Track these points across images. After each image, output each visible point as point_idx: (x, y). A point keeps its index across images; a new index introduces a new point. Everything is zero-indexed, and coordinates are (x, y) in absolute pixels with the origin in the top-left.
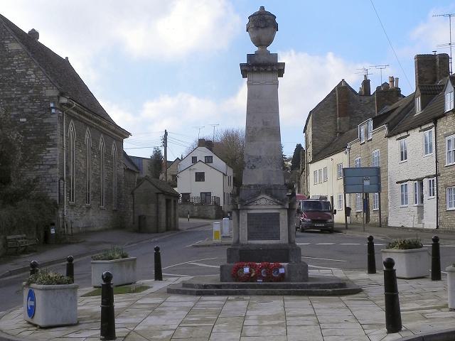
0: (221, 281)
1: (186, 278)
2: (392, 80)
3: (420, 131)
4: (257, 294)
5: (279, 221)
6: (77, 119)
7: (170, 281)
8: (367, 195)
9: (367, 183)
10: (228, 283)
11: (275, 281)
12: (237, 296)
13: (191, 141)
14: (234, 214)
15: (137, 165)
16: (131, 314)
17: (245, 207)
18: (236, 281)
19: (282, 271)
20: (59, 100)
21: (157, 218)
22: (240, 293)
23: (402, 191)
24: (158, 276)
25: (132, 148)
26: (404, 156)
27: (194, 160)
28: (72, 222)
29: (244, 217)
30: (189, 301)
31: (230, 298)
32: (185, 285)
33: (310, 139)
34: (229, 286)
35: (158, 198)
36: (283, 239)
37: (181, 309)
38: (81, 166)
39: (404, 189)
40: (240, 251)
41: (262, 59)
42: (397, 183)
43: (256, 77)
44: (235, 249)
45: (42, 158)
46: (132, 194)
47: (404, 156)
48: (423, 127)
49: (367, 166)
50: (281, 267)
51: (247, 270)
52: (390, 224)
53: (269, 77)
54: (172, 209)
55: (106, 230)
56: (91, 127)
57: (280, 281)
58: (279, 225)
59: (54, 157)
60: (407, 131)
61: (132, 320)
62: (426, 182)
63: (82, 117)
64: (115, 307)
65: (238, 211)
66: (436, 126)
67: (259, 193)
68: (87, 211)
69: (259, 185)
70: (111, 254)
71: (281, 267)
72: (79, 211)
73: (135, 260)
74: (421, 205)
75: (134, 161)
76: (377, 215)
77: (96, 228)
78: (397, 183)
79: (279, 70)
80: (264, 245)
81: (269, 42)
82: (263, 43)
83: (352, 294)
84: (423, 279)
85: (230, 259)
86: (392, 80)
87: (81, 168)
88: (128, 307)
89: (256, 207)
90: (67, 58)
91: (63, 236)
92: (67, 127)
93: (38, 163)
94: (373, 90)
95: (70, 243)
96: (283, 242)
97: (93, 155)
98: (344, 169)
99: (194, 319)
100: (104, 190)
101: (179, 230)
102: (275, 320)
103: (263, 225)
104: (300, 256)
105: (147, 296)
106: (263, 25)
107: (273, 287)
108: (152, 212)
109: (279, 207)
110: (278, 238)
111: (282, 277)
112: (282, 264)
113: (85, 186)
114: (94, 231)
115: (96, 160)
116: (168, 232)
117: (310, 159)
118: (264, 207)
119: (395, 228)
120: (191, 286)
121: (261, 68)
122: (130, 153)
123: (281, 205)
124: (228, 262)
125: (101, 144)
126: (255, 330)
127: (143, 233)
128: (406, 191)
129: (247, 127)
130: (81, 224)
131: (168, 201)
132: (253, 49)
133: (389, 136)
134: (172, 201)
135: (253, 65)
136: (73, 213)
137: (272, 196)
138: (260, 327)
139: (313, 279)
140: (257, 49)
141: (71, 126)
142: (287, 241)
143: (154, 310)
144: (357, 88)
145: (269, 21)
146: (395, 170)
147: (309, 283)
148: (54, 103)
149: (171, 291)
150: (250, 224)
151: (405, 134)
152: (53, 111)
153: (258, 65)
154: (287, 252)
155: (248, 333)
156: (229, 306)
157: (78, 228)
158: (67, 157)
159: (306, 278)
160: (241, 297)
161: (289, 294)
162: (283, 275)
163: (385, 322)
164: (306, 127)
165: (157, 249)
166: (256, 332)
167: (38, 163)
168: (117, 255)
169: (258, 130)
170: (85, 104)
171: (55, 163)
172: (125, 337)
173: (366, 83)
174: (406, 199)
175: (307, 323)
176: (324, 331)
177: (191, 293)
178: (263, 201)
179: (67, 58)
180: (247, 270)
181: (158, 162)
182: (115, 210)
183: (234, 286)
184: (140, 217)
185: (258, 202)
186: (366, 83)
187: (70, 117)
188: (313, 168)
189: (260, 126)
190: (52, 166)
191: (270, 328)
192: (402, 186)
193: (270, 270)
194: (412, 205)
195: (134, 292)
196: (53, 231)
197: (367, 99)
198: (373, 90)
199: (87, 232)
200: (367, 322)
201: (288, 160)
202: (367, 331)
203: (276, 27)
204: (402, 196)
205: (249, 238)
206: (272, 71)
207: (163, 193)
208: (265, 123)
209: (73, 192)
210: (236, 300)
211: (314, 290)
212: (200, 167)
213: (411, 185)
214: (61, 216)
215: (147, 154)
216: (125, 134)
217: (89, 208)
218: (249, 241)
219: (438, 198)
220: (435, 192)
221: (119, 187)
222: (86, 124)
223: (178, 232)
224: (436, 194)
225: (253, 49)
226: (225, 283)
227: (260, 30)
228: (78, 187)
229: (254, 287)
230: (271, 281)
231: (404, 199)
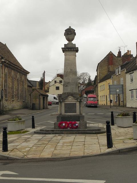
0: (55, 129)
1: (43, 127)
2: (128, 51)
4: (67, 133)
5: (76, 106)
6: (8, 67)
7: (38, 129)
8: (119, 95)
9: (118, 91)
10: (56, 129)
11: (74, 129)
12: (54, 135)
13: (55, 75)
14: (60, 103)
15: (33, 84)
16: (17, 142)
17: (64, 101)
18: (60, 129)
19: (77, 125)
21: (40, 104)
22: (60, 133)
23: (131, 94)
24: (33, 127)
25: (31, 77)
26: (132, 80)
27: (55, 82)
28: (6, 106)
29: (63, 104)
30: (40, 136)
31: (57, 135)
32: (41, 130)
34: (57, 131)
35: (40, 97)
36: (78, 113)
37: (36, 139)
38: (10, 85)
39: (132, 93)
40: (62, 117)
41: (70, 46)
42: (130, 90)
43: (68, 53)
44: (60, 117)
46: (30, 95)
47: (132, 80)
50: (77, 123)
51: (64, 124)
52: (127, 106)
53: (72, 53)
54: (46, 101)
55: (20, 109)
56: (14, 70)
57: (76, 129)
58: (76, 107)
60: (133, 71)
61: (16, 144)
63: (10, 66)
64: (8, 141)
65: (61, 102)
67: (68, 96)
68: (12, 102)
69: (69, 93)
70: (15, 119)
71: (77, 123)
72: (9, 102)
73: (24, 121)
75: (32, 83)
76: (122, 102)
77: (16, 108)
78: (130, 90)
79: (77, 50)
81: (73, 39)
82: (70, 40)
83: (103, 133)
84: (131, 128)
85: (58, 121)
88: (17, 139)
89: (68, 101)
91: (2, 112)
92: (5, 70)
95: (5, 114)
96: (78, 114)
99: (39, 143)
101: (48, 109)
102: (69, 143)
103: (70, 108)
104: (84, 118)
105: (26, 135)
107: (73, 131)
108: (38, 102)
109: (76, 101)
111: (77, 127)
112: (77, 122)
114: (15, 110)
116: (44, 110)
117: (99, 82)
118: (71, 101)
119: (129, 108)
120: (43, 131)
121: (70, 49)
122: (29, 79)
124: (57, 121)
125: (18, 76)
126: (60, 147)
127: (34, 110)
128: (133, 94)
129: (64, 71)
130: (10, 107)
131: (44, 98)
132: (66, 42)
133: (126, 73)
134: (46, 98)
135: (66, 48)
137: (73, 97)
138: (63, 146)
139: (89, 127)
140: (68, 42)
141: (6, 70)
142: (79, 114)
143: (26, 140)
144: (116, 54)
145: (72, 32)
147: (86, 129)
149: (35, 133)
151: (132, 72)
153: (68, 48)
154: (79, 118)
155: (57, 149)
156: (55, 138)
157: (9, 108)
159: (86, 127)
160: (61, 135)
161: (79, 133)
162: (77, 126)
163: (107, 144)
164: (97, 70)
165: (33, 117)
166: (60, 148)
168: (17, 119)
169: (68, 72)
170: (12, 62)
172: (12, 151)
173: (120, 53)
174: (133, 96)
175: (80, 144)
176: (101, 148)
177: (43, 133)
178: (70, 99)
180: (64, 124)
181: (42, 83)
183: (59, 131)
184: (33, 104)
186: (120, 53)
187: (6, 66)
188: (99, 85)
189: (69, 71)
191: (66, 147)
193: (73, 124)
195: (22, 133)
197: (120, 59)
198: (122, 54)
199: (13, 110)
200: (103, 144)
201: (92, 82)
202: (101, 148)
203: (75, 34)
204: (131, 95)
205: (65, 113)
206: (74, 51)
207: (42, 95)
208: (71, 70)
209: (7, 95)
210: (59, 136)
211: (88, 132)
212: (57, 85)
214: (2, 104)
215: (38, 79)
216: (28, 73)
217: (13, 101)
218: (65, 114)
221: (26, 92)
222: (12, 69)
223: (47, 110)
225: (66, 42)
226: (55, 130)
227: (69, 35)
228: (9, 93)
229: (66, 131)
230: (73, 129)
231: (132, 96)
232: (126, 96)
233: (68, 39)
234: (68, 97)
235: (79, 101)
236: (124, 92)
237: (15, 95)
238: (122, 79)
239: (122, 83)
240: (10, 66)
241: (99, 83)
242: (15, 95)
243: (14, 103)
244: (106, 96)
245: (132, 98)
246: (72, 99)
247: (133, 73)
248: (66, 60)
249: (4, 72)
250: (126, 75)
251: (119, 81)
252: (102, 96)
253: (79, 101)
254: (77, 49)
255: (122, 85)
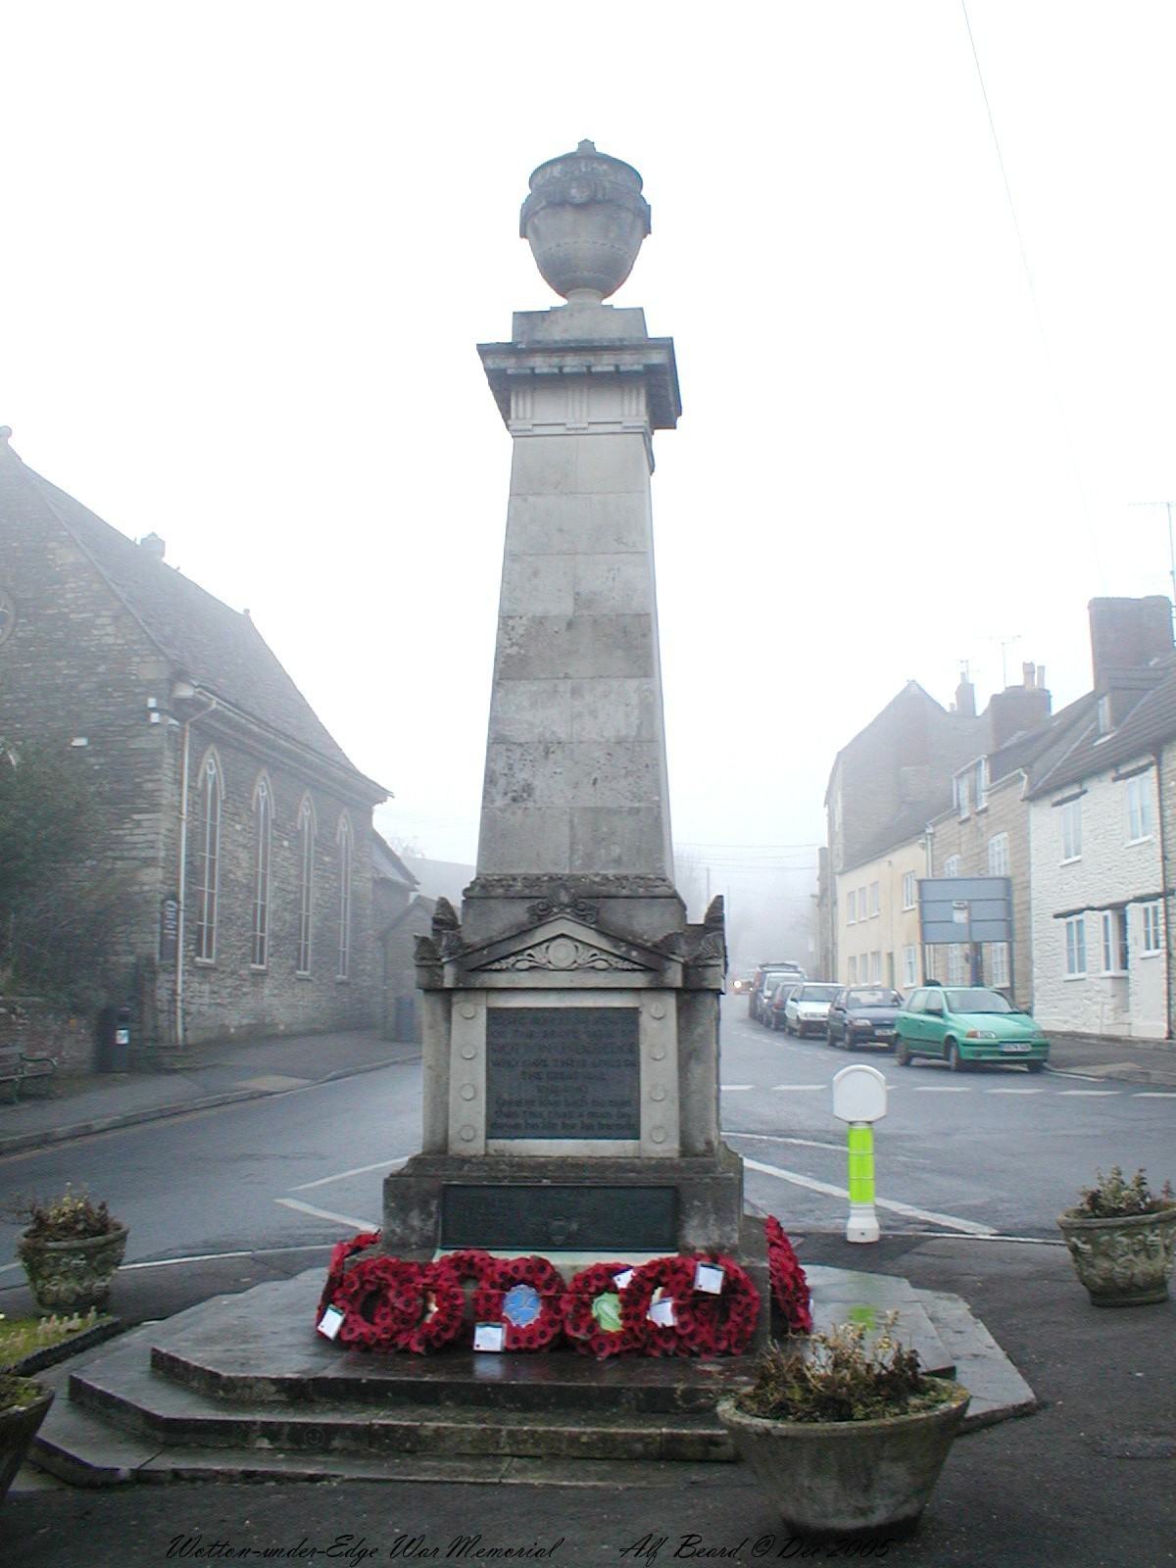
3: (1115, 780)
5: (633, 1049)
8: (977, 947)
20: (171, 691)
33: (839, 819)
36: (657, 1137)
38: (238, 865)
42: (1057, 916)
45: (119, 840)
48: (1123, 770)
49: (976, 876)
58: (635, 1065)
59: (151, 837)
60: (1079, 780)
62: (1134, 913)
66: (1159, 763)
72: (229, 982)
74: (1123, 973)
80: (563, 1163)
86: (1029, 670)
87: (240, 873)
90: (247, 611)
93: (110, 853)
94: (982, 704)
97: (280, 839)
98: (920, 882)
100: (311, 931)
106: (588, 209)
109: (639, 980)
110: (630, 1129)
113: (249, 918)
115: (288, 854)
123: (646, 969)
128: (1080, 941)
130: (235, 1019)
133: (1033, 798)
136: (206, 987)
144: (947, 699)
146: (1050, 887)
148: (159, 697)
150: (498, 1057)
151: (1075, 790)
152: (155, 717)
158: (191, 839)
167: (110, 853)
171: (150, 853)
173: (966, 692)
178: (561, 954)
179: (247, 611)
182: (342, 983)
185: (539, 955)
186: (966, 692)
190: (149, 862)
192: (1070, 923)
194: (1099, 970)
196: (122, 1037)
205: (494, 1130)
213: (1093, 922)
216: (380, 794)
219: (1169, 955)
220: (1162, 937)
224: (1163, 944)
228: (227, 921)
232: (1028, 958)
233: (558, 273)
234: (540, 935)
235: (679, 983)
236: (1017, 925)
237: (275, 936)
238: (999, 845)
239: (999, 862)
240: (247, 741)
241: (841, 874)
242: (275, 936)
243: (267, 992)
244: (890, 956)
245: (1071, 970)
246: (585, 956)
247: (1076, 797)
248: (525, 485)
249: (194, 775)
250: (1027, 812)
251: (982, 853)
252: (864, 956)
253: (679, 983)
254: (657, 358)
255: (1007, 881)
